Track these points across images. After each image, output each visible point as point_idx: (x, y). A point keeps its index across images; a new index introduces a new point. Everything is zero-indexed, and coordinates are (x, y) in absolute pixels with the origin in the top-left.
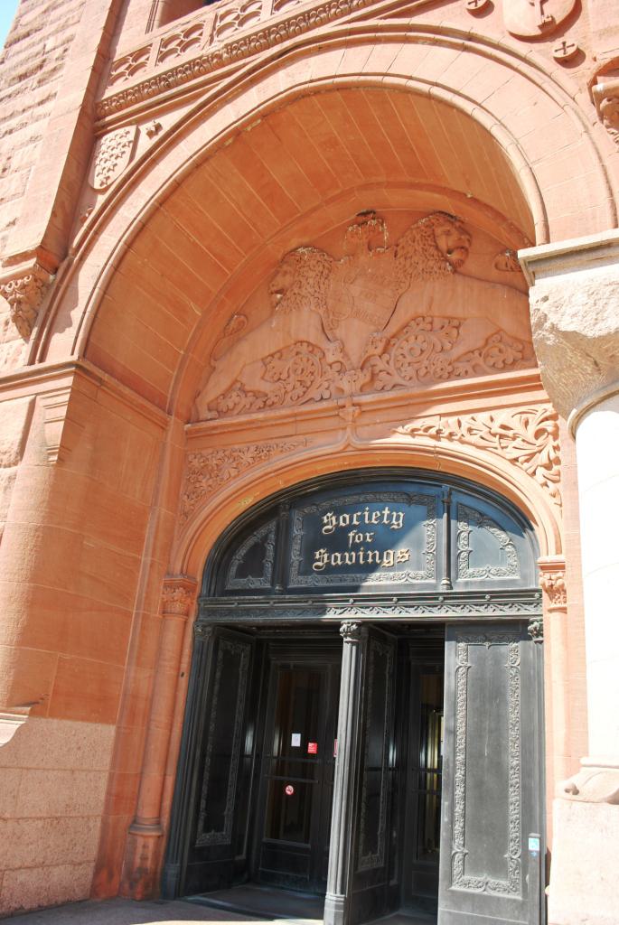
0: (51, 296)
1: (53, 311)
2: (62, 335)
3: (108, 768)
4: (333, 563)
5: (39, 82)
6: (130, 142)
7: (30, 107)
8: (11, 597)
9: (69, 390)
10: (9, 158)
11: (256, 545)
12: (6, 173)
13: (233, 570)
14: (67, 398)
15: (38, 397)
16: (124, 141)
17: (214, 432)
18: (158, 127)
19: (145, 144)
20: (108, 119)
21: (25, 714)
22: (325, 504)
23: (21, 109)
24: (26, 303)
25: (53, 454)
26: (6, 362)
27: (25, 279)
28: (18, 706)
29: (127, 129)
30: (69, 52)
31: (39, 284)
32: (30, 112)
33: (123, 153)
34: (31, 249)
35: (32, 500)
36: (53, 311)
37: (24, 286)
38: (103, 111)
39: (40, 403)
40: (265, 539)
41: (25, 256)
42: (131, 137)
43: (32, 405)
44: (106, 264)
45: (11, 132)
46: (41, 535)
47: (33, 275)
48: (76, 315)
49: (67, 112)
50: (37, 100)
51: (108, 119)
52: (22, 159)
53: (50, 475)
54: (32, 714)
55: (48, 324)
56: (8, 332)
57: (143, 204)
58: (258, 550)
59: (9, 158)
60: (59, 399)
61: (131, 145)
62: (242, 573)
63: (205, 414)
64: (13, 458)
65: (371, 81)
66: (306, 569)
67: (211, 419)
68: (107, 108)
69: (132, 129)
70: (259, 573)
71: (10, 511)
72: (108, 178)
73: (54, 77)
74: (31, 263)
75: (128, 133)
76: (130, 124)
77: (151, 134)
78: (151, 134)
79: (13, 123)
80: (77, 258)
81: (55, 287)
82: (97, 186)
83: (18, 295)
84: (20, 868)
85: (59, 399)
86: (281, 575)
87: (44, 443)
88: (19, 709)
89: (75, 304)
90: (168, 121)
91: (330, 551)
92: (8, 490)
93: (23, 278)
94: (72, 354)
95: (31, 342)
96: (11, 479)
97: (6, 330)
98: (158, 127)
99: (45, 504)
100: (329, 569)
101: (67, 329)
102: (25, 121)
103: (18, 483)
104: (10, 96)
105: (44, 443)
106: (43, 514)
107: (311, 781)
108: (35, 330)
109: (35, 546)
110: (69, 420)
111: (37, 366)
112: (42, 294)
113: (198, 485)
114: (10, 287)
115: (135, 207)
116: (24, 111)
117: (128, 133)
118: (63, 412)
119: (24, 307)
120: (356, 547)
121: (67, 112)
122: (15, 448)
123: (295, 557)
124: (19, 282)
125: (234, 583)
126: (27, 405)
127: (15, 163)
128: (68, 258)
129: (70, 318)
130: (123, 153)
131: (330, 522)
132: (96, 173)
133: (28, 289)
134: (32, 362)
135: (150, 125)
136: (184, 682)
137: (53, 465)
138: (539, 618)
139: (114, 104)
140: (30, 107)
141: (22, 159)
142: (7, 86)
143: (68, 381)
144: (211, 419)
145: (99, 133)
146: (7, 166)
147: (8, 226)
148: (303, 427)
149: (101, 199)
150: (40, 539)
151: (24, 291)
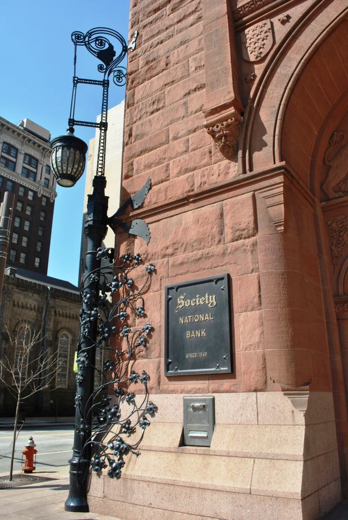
0: (244, 129)
1: (248, 139)
2: (260, 153)
3: (334, 419)
4: (198, 304)
5: (172, 10)
6: (269, 29)
7: (171, 26)
8: (279, 318)
9: (282, 184)
10: (168, 57)
12: (169, 66)
14: (282, 189)
15: (256, 193)
16: (265, 29)
17: (344, 205)
18: (288, 17)
19: (281, 31)
20: (244, 19)
21: (307, 390)
23: (164, 28)
24: (231, 136)
25: (280, 226)
26: (219, 176)
27: (229, 120)
28: (301, 386)
29: (264, 22)
30: (131, 4)
31: (238, 123)
32: (172, 28)
33: (267, 36)
34: (229, 101)
35: (274, 256)
36: (248, 139)
37: (228, 125)
38: (239, 15)
41: (225, 107)
42: (269, 26)
43: (254, 197)
44: (280, 105)
45: (162, 42)
46: (286, 277)
47: (235, 117)
48: (268, 138)
49: (217, 19)
50: (176, 20)
51: (244, 19)
52: (179, 56)
53: (280, 239)
54: (310, 390)
55: (248, 147)
56: (212, 157)
57: (296, 64)
59: (168, 57)
61: (271, 31)
63: (332, 195)
64: (251, 232)
67: (339, 197)
68: (241, 12)
69: (268, 21)
71: (260, 265)
72: (261, 53)
73: (183, 5)
74: (232, 110)
75: (265, 24)
76: (267, 18)
77: (283, 22)
78: (283, 22)
79: (162, 36)
80: (255, 104)
81: (245, 124)
82: (252, 58)
83: (225, 132)
84: (199, 488)
87: (271, 220)
88: (303, 388)
89: (264, 132)
90: (296, 12)
92: (254, 252)
93: (227, 120)
94: (275, 163)
95: (240, 160)
96: (254, 245)
97: (211, 157)
98: (288, 17)
99: (283, 257)
101: (264, 148)
102: (171, 34)
103: (259, 247)
104: (151, 23)
105: (271, 220)
106: (283, 264)
108: (240, 153)
109: (284, 285)
110: (286, 203)
111: (249, 174)
112: (239, 129)
113: (341, 238)
114: (217, 127)
115: (290, 67)
116: (167, 29)
117: (265, 24)
118: (281, 198)
119: (230, 139)
121: (217, 19)
122: (252, 225)
124: (225, 123)
126: (251, 198)
127: (173, 59)
128: (249, 105)
129: (264, 142)
130: (267, 36)
132: (249, 53)
133: (231, 126)
135: (282, 16)
137: (281, 233)
139: (247, 9)
140: (171, 26)
141: (179, 56)
142: (146, 17)
143: (280, 179)
144: (339, 197)
145: (240, 28)
146: (168, 62)
147: (184, 96)
149: (259, 70)
150: (286, 279)
151: (229, 128)
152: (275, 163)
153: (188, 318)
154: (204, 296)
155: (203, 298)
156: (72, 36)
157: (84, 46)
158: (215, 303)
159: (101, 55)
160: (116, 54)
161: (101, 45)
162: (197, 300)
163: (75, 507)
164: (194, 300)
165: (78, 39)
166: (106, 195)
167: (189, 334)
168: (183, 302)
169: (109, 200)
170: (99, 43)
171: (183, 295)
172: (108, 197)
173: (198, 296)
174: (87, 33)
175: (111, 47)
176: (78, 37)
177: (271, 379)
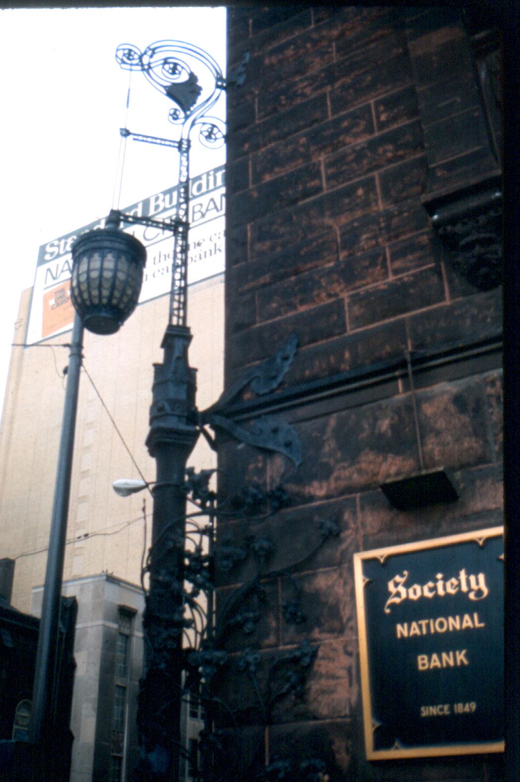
94: (46, 283)
152: (46, 283)
153: (420, 627)
154: (457, 576)
155: (454, 581)
156: (118, 50)
157: (176, 150)
158: (486, 591)
159: (173, 92)
160: (202, 92)
161: (174, 73)
162: (440, 584)
163: (212, 636)
164: (431, 584)
165: (128, 59)
166: (192, 363)
167: (426, 661)
168: (402, 590)
169: (199, 376)
170: (170, 68)
171: (402, 576)
172: (195, 370)
173: (439, 576)
174: (148, 48)
175: (193, 78)
176: (129, 54)
177: (211, 240)
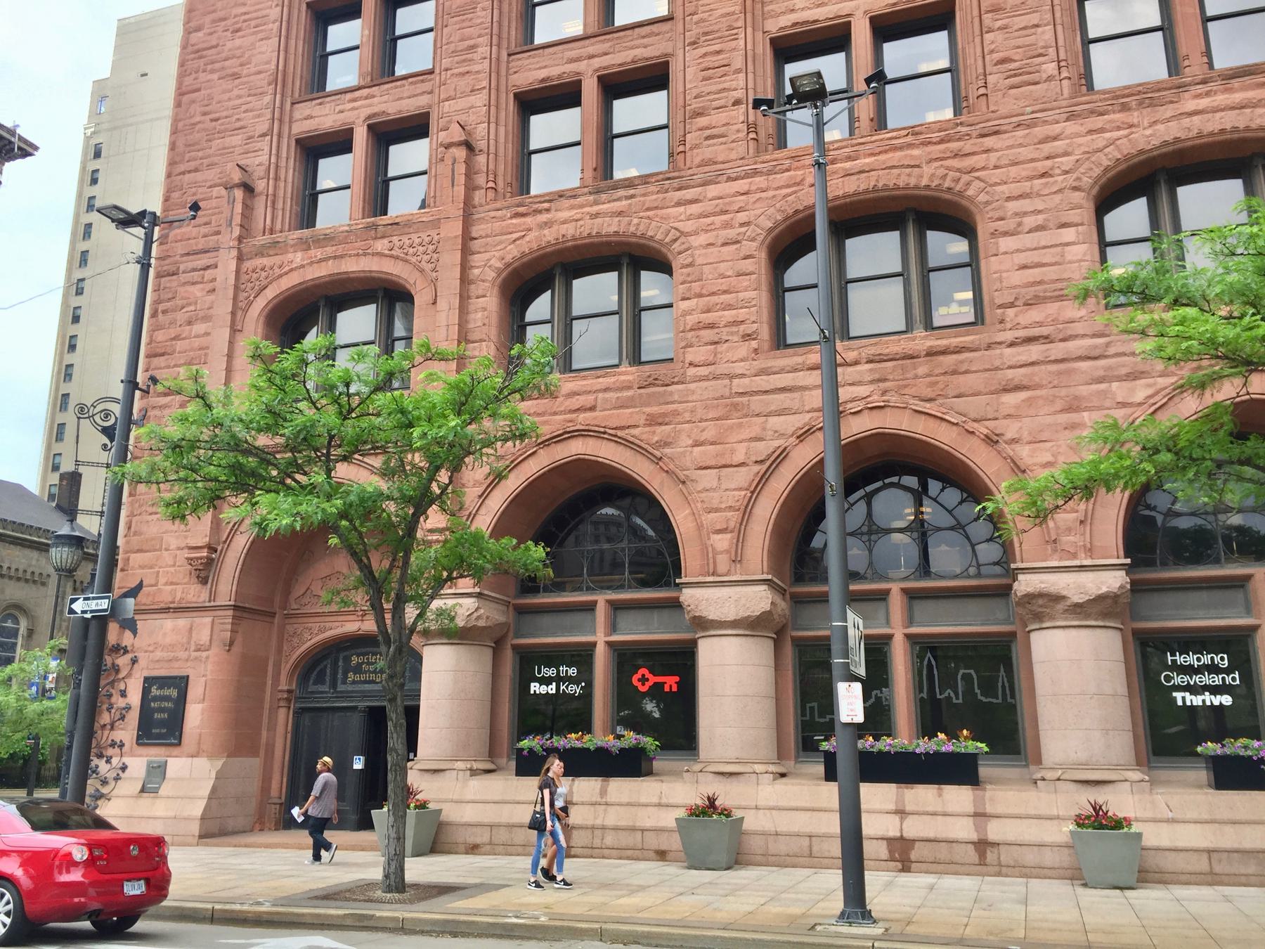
11: (321, 670)
13: (311, 681)
22: (353, 651)
39: (217, 621)
40: (326, 666)
43: (213, 622)
58: (322, 672)
60: (226, 621)
62: (315, 683)
65: (289, 761)
66: (344, 682)
70: (323, 683)
71: (208, 673)
85: (226, 621)
86: (334, 685)
91: (355, 674)
100: (354, 682)
103: (211, 660)
107: (601, 661)
120: (365, 672)
123: (340, 676)
125: (312, 688)
131: (355, 660)
134: (210, 601)
136: (289, 736)
138: (1113, 300)
148: (341, 618)
